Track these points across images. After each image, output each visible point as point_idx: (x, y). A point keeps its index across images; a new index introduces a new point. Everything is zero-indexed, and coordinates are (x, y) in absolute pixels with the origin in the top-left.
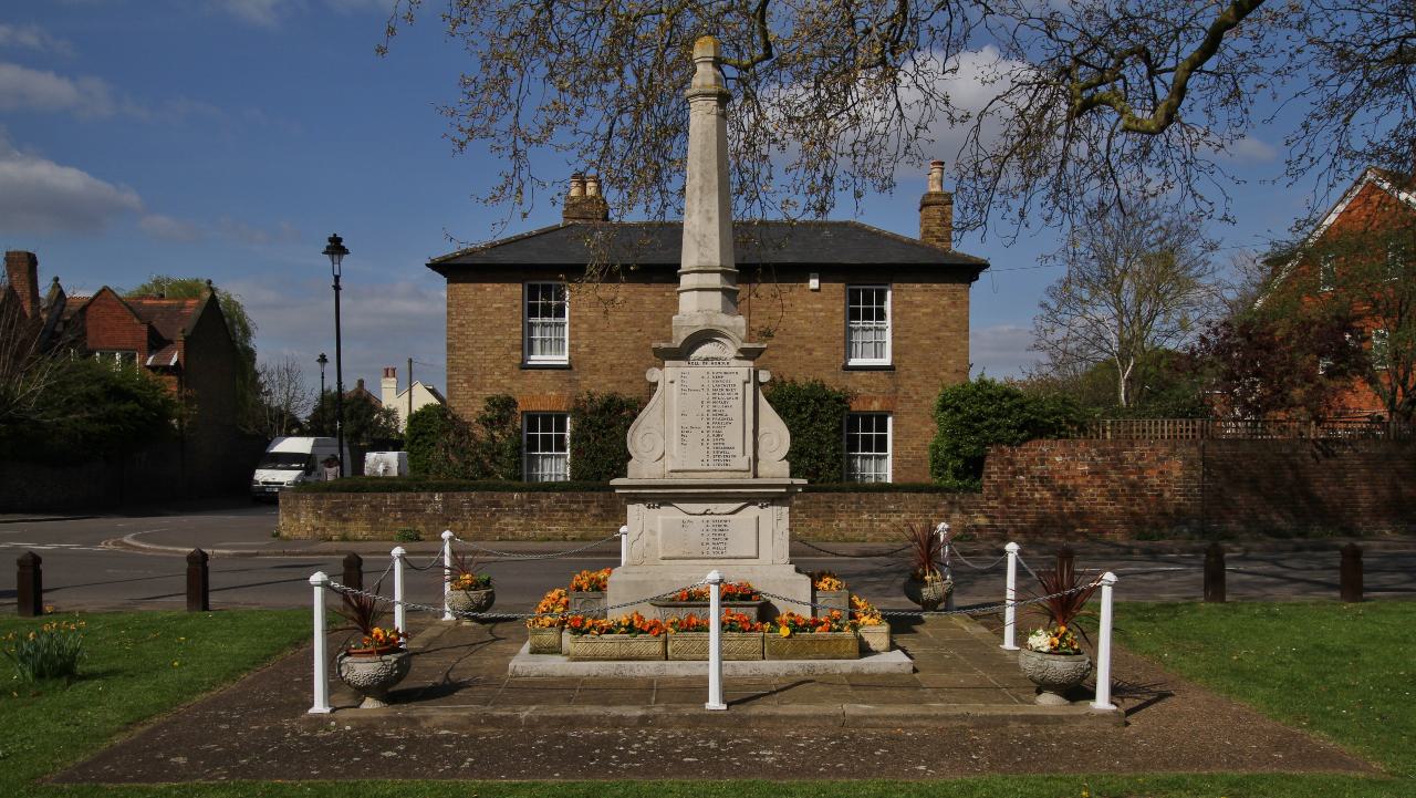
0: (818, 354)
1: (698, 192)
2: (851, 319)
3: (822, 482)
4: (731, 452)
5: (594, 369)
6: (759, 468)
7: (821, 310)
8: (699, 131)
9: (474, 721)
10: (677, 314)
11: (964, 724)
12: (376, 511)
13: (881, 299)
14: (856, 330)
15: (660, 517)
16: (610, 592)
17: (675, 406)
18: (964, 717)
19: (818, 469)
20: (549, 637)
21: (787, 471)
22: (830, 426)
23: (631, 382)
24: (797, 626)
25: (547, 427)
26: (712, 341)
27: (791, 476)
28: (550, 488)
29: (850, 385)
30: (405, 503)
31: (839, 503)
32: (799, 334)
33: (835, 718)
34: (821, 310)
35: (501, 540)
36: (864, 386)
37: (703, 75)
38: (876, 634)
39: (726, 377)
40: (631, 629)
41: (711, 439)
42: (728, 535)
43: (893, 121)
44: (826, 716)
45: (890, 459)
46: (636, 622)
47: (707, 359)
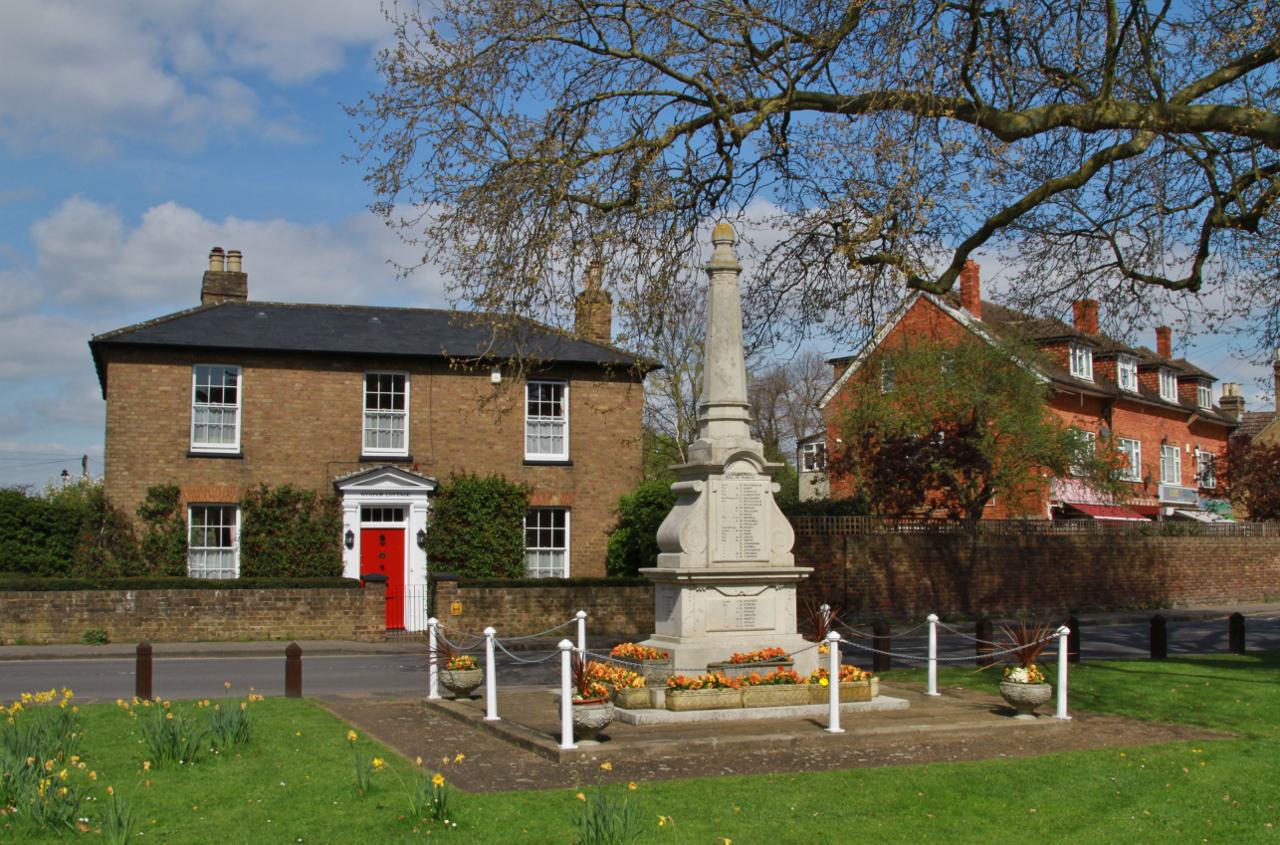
4: (757, 547)
5: (269, 459)
9: (682, 750)
12: (59, 611)
13: (558, 395)
21: (793, 562)
23: (307, 473)
25: (545, 522)
29: (531, 480)
30: (92, 601)
32: (480, 427)
33: (913, 733)
35: (200, 641)
36: (544, 481)
39: (754, 488)
44: (907, 733)
45: (567, 554)
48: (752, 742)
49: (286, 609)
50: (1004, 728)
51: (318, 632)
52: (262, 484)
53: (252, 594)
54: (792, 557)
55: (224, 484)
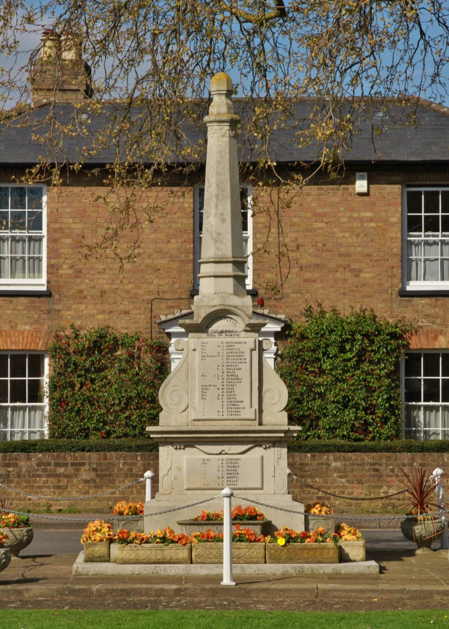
0: (366, 276)
1: (214, 199)
2: (410, 230)
3: (373, 439)
5: (80, 296)
6: (264, 418)
7: (371, 220)
8: (215, 150)
10: (198, 294)
11: (402, 596)
14: (418, 244)
15: (185, 456)
16: (144, 512)
17: (197, 368)
18: (402, 591)
19: (367, 424)
20: (101, 549)
21: (286, 420)
22: (383, 369)
23: (127, 313)
24: (290, 539)
26: (225, 317)
27: (289, 424)
28: (27, 447)
31: (387, 465)
32: (342, 250)
33: (310, 591)
34: (371, 220)
36: (427, 316)
37: (219, 105)
38: (353, 544)
39: (237, 346)
40: (164, 540)
41: (225, 394)
42: (239, 470)
43: (418, 51)
44: (304, 590)
46: (168, 535)
47: (222, 332)
48: (132, 590)
49: (68, 476)
50: (421, 592)
51: (105, 503)
52: (72, 326)
53: (29, 459)
54: (285, 415)
55: (27, 328)
